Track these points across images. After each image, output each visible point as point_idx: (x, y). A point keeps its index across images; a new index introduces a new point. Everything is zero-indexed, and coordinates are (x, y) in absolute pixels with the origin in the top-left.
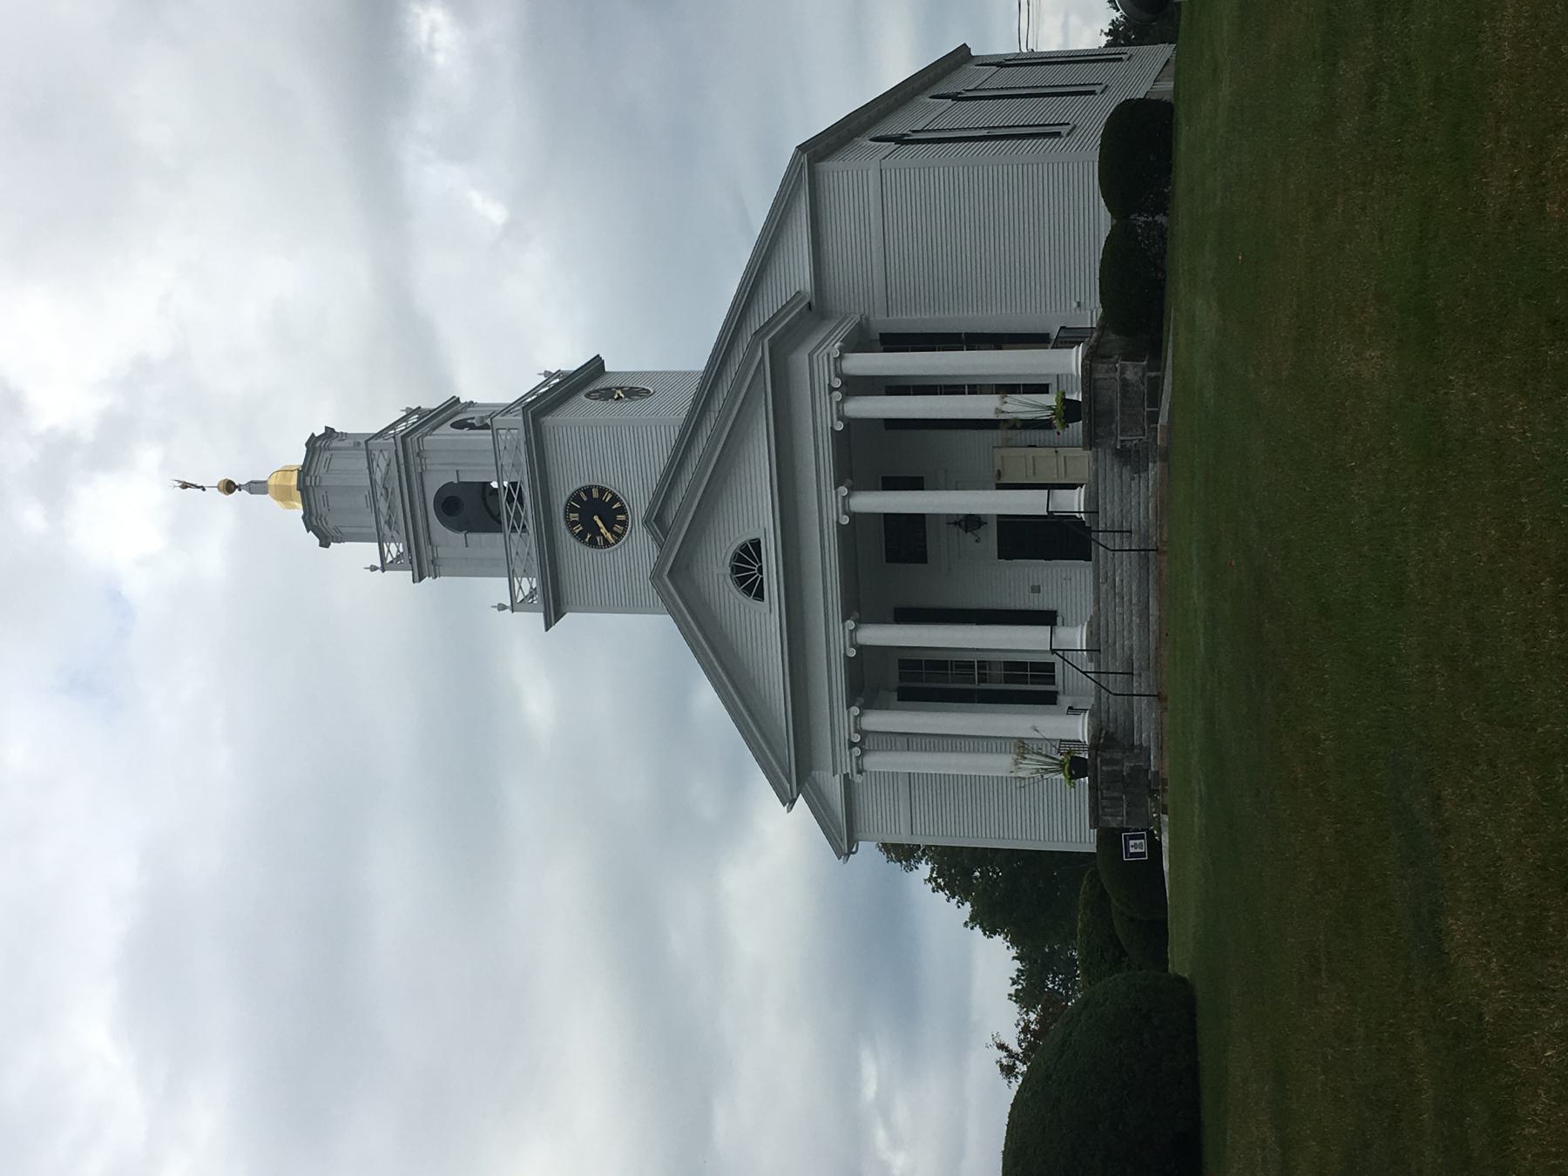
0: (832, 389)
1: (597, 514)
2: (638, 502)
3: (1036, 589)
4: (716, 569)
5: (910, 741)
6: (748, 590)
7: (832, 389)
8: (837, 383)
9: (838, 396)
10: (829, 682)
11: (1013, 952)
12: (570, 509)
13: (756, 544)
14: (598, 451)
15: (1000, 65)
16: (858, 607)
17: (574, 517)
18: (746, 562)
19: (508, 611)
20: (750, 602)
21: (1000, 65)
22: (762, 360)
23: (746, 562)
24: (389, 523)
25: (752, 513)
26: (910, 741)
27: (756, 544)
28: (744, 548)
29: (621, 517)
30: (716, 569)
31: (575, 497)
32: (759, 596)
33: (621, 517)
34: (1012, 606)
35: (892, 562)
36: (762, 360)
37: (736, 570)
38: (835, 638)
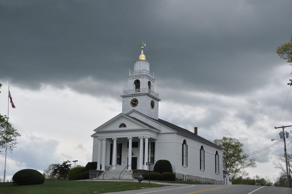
0: (143, 137)
1: (134, 103)
2: (136, 108)
3: (124, 162)
4: (123, 121)
5: (102, 145)
6: (120, 125)
7: (143, 137)
8: (144, 138)
9: (143, 138)
10: (109, 136)
11: (73, 166)
12: (135, 99)
13: (126, 127)
14: (144, 102)
15: (106, 154)
16: (119, 140)
17: (134, 100)
18: (123, 125)
19: (123, 90)
20: (119, 126)
21: (106, 154)
22: (146, 128)
23: (123, 125)
24: (135, 73)
25: (130, 126)
26: (102, 145)
27: (126, 127)
28: (125, 125)
29: (134, 106)
30: (123, 121)
31: (137, 100)
32: (120, 127)
33: (134, 106)
34: (122, 159)
35: (122, 144)
36: (146, 128)
37: (123, 124)
38: (114, 137)
